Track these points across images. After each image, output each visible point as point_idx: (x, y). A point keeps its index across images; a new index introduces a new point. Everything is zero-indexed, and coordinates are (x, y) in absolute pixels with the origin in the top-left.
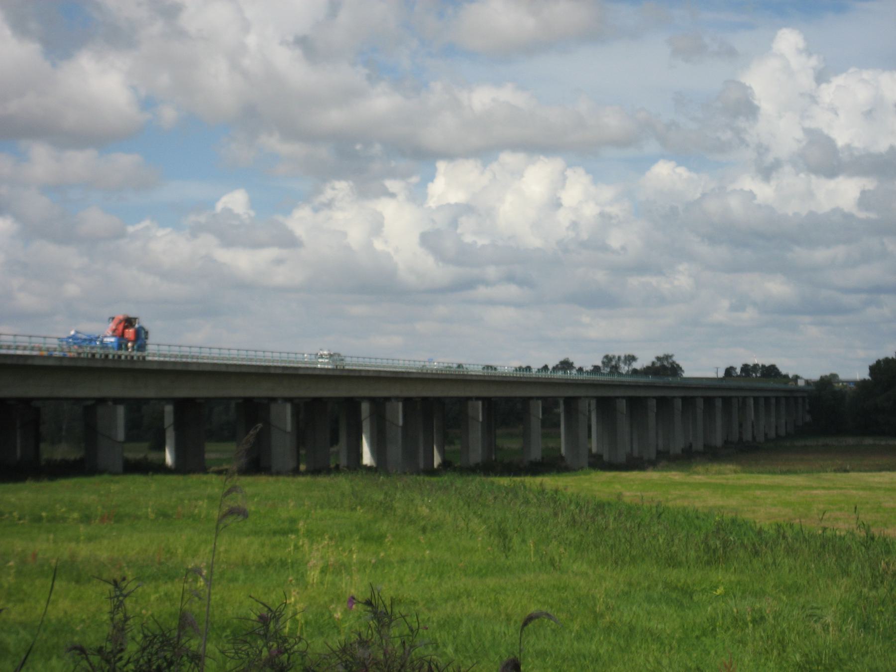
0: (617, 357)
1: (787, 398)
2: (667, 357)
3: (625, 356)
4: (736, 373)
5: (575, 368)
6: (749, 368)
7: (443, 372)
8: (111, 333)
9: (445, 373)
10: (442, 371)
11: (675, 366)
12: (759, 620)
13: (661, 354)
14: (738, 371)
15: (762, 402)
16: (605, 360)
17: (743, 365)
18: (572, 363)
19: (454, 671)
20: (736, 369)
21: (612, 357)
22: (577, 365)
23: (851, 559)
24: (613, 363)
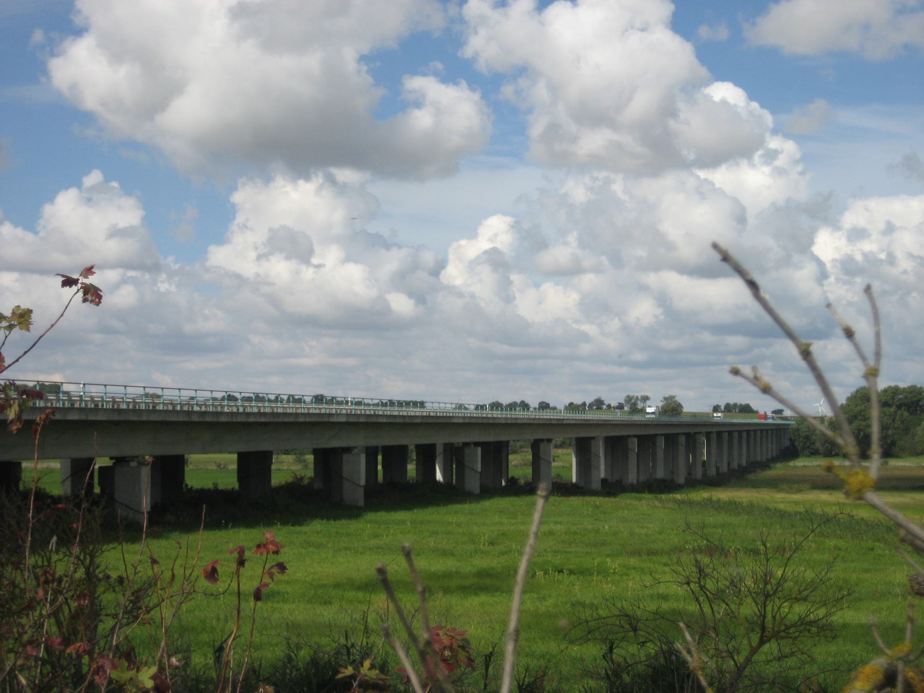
0: (635, 397)
1: (776, 429)
2: (672, 397)
3: (641, 396)
4: (721, 409)
5: (605, 404)
6: (731, 406)
7: (438, 414)
8: (147, 392)
9: (441, 415)
10: (436, 412)
13: (667, 396)
14: (722, 408)
19: (586, 692)
22: (606, 402)
24: (633, 401)
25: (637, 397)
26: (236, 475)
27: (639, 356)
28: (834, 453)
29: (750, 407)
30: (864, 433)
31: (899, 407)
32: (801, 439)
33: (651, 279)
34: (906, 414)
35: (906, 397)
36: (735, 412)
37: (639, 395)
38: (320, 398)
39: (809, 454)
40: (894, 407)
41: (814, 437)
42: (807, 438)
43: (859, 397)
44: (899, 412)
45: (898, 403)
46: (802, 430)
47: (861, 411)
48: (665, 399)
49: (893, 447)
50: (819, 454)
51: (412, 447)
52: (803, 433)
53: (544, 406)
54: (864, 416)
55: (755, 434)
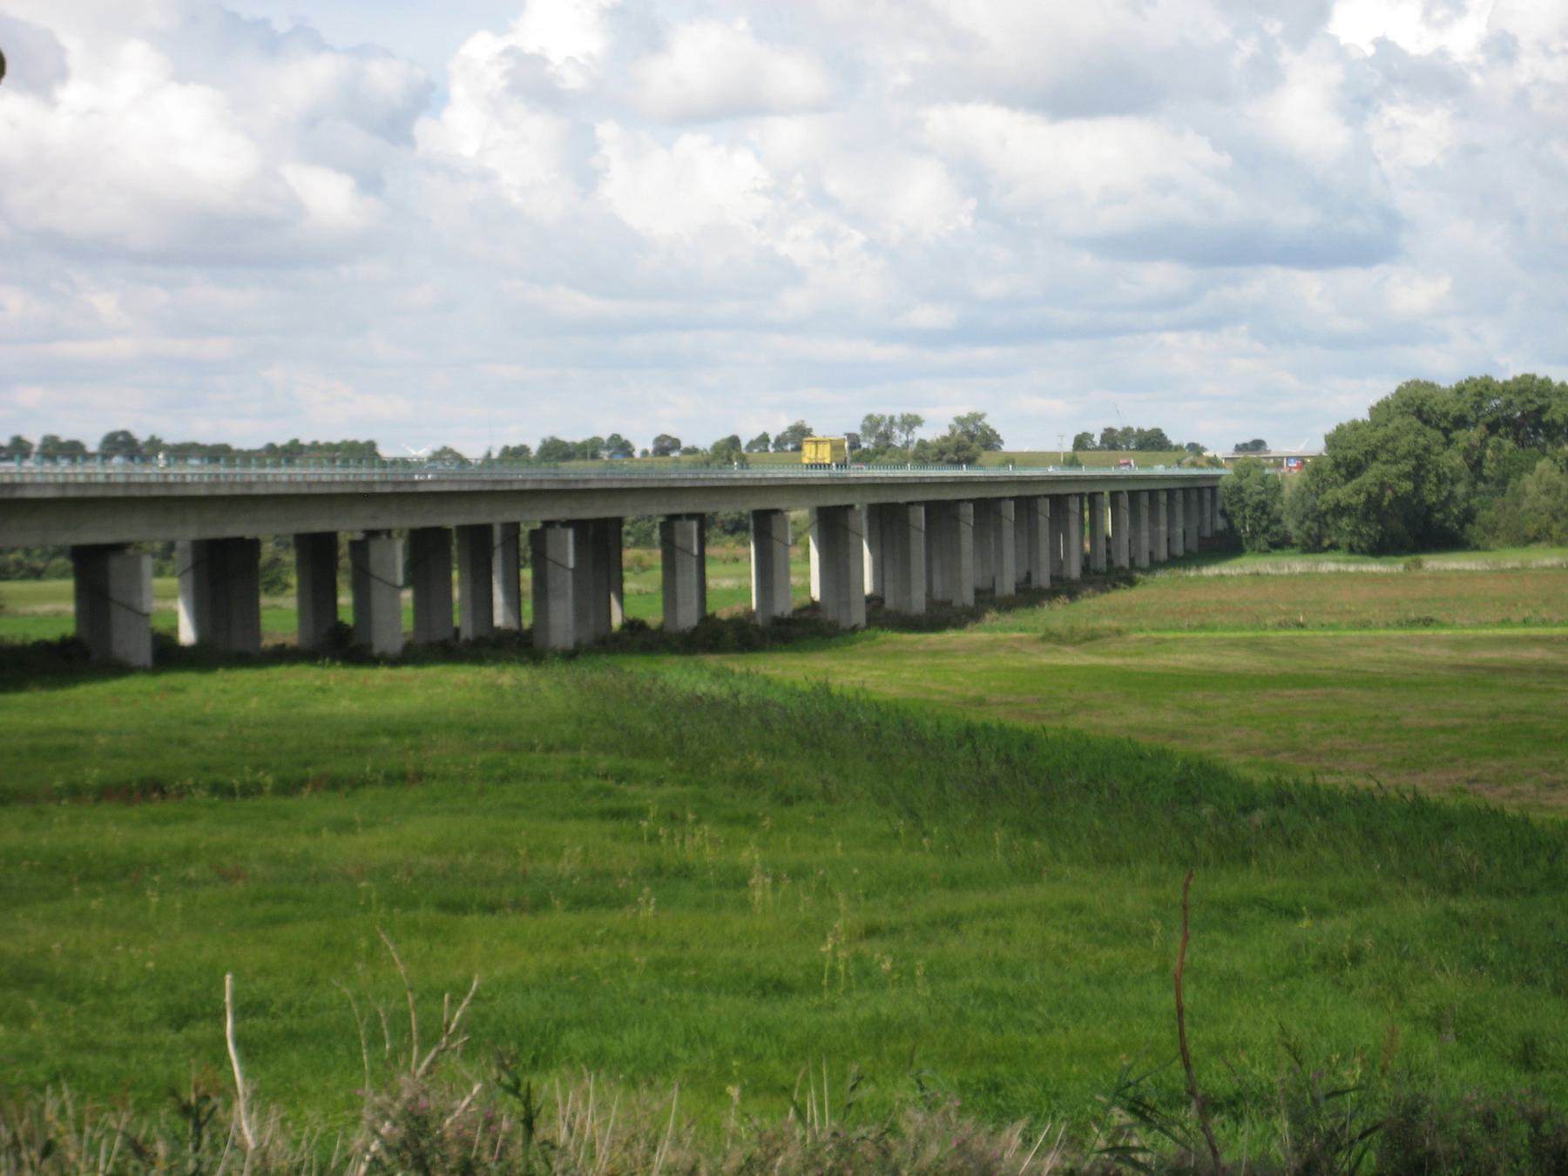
2: (976, 418)
3: (902, 416)
4: (1093, 443)
11: (988, 432)
12: (1500, 923)
13: (964, 413)
14: (1097, 440)
15: (1145, 499)
16: (867, 423)
17: (1105, 430)
18: (811, 429)
20: (1093, 436)
21: (879, 418)
23: (499, 772)
24: (882, 429)
25: (892, 420)
26: (261, 606)
27: (928, 316)
28: (1326, 542)
29: (1162, 435)
30: (1395, 493)
31: (1493, 428)
32: (1248, 512)
33: (942, 121)
34: (1509, 444)
35: (1509, 404)
36: (1128, 449)
37: (897, 412)
38: (120, 438)
39: (1266, 547)
40: (1481, 428)
41: (1278, 506)
42: (1262, 507)
43: (1397, 407)
44: (1492, 441)
45: (1489, 419)
46: (1248, 491)
47: (1387, 440)
48: (960, 421)
49: (1468, 526)
50: (1293, 546)
51: (1106, 494)
52: (1251, 495)
53: (666, 446)
54: (1394, 454)
55: (1201, 498)
